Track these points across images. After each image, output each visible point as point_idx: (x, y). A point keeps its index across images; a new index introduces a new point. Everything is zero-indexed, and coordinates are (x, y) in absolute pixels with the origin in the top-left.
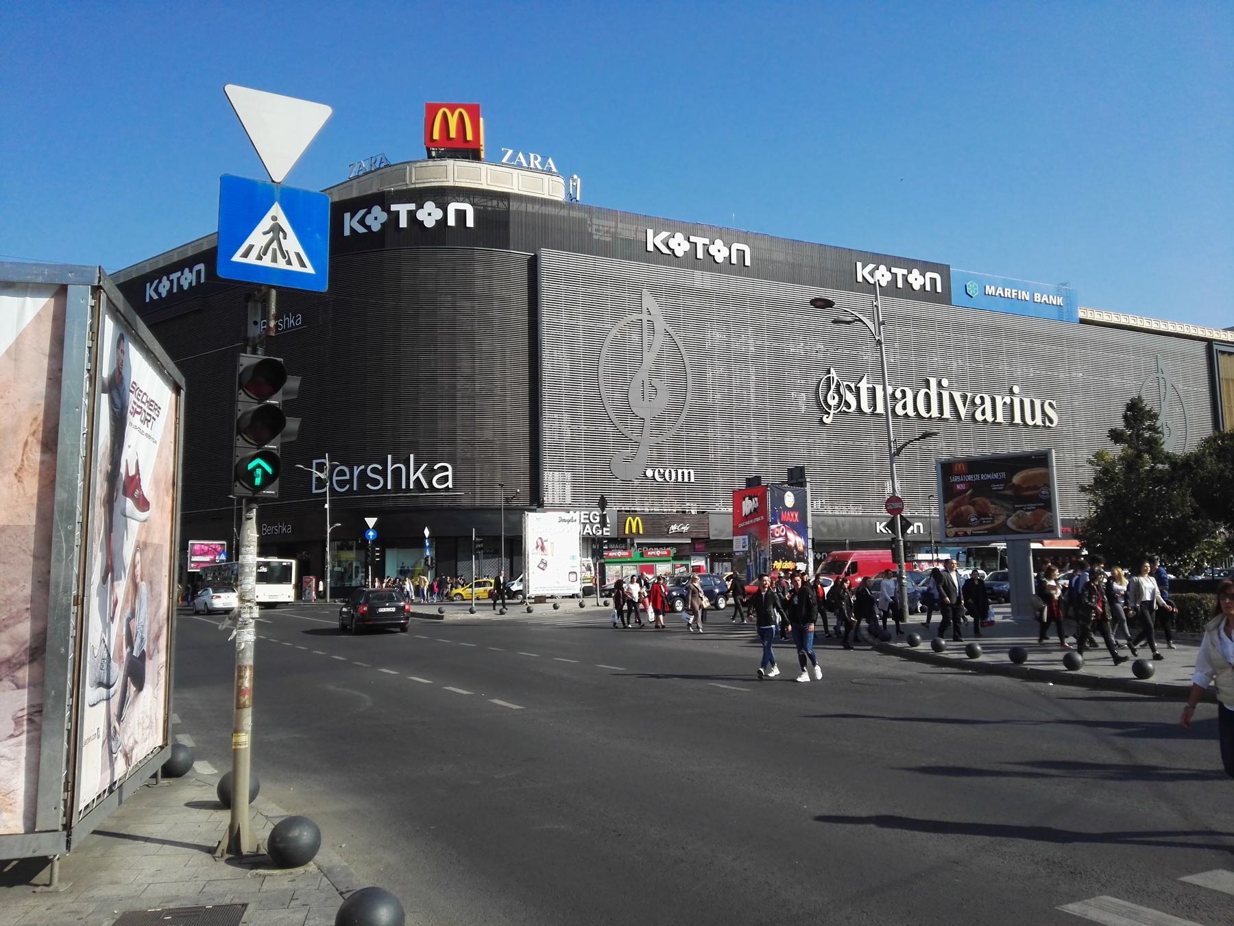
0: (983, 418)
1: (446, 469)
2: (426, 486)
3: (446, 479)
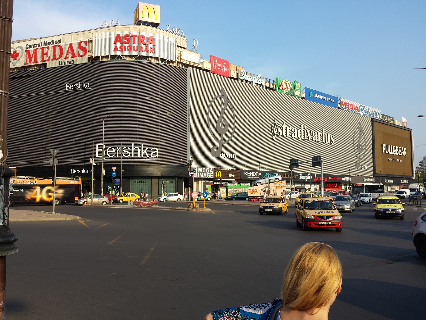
0: (294, 137)
1: (156, 150)
2: (148, 156)
3: (155, 154)
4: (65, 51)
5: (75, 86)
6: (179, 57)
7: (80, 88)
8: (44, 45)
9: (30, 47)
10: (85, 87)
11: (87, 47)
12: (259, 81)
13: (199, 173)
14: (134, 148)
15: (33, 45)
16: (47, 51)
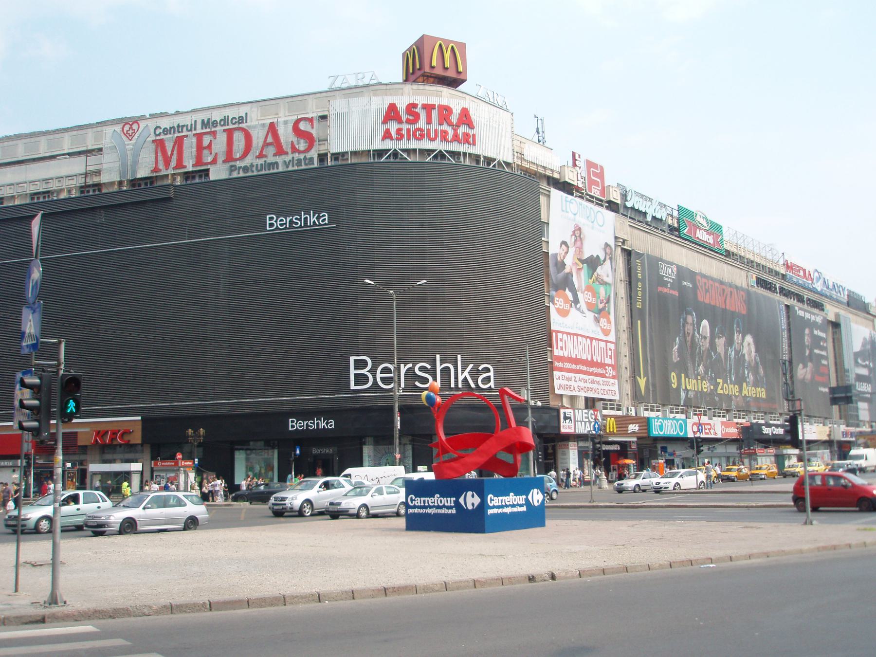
2: (473, 386)
3: (325, 220)
5: (291, 222)
6: (519, 156)
7: (303, 225)
8: (202, 129)
9: (166, 131)
10: (318, 224)
11: (315, 133)
12: (647, 207)
13: (577, 422)
14: (441, 365)
15: (174, 127)
16: (211, 142)
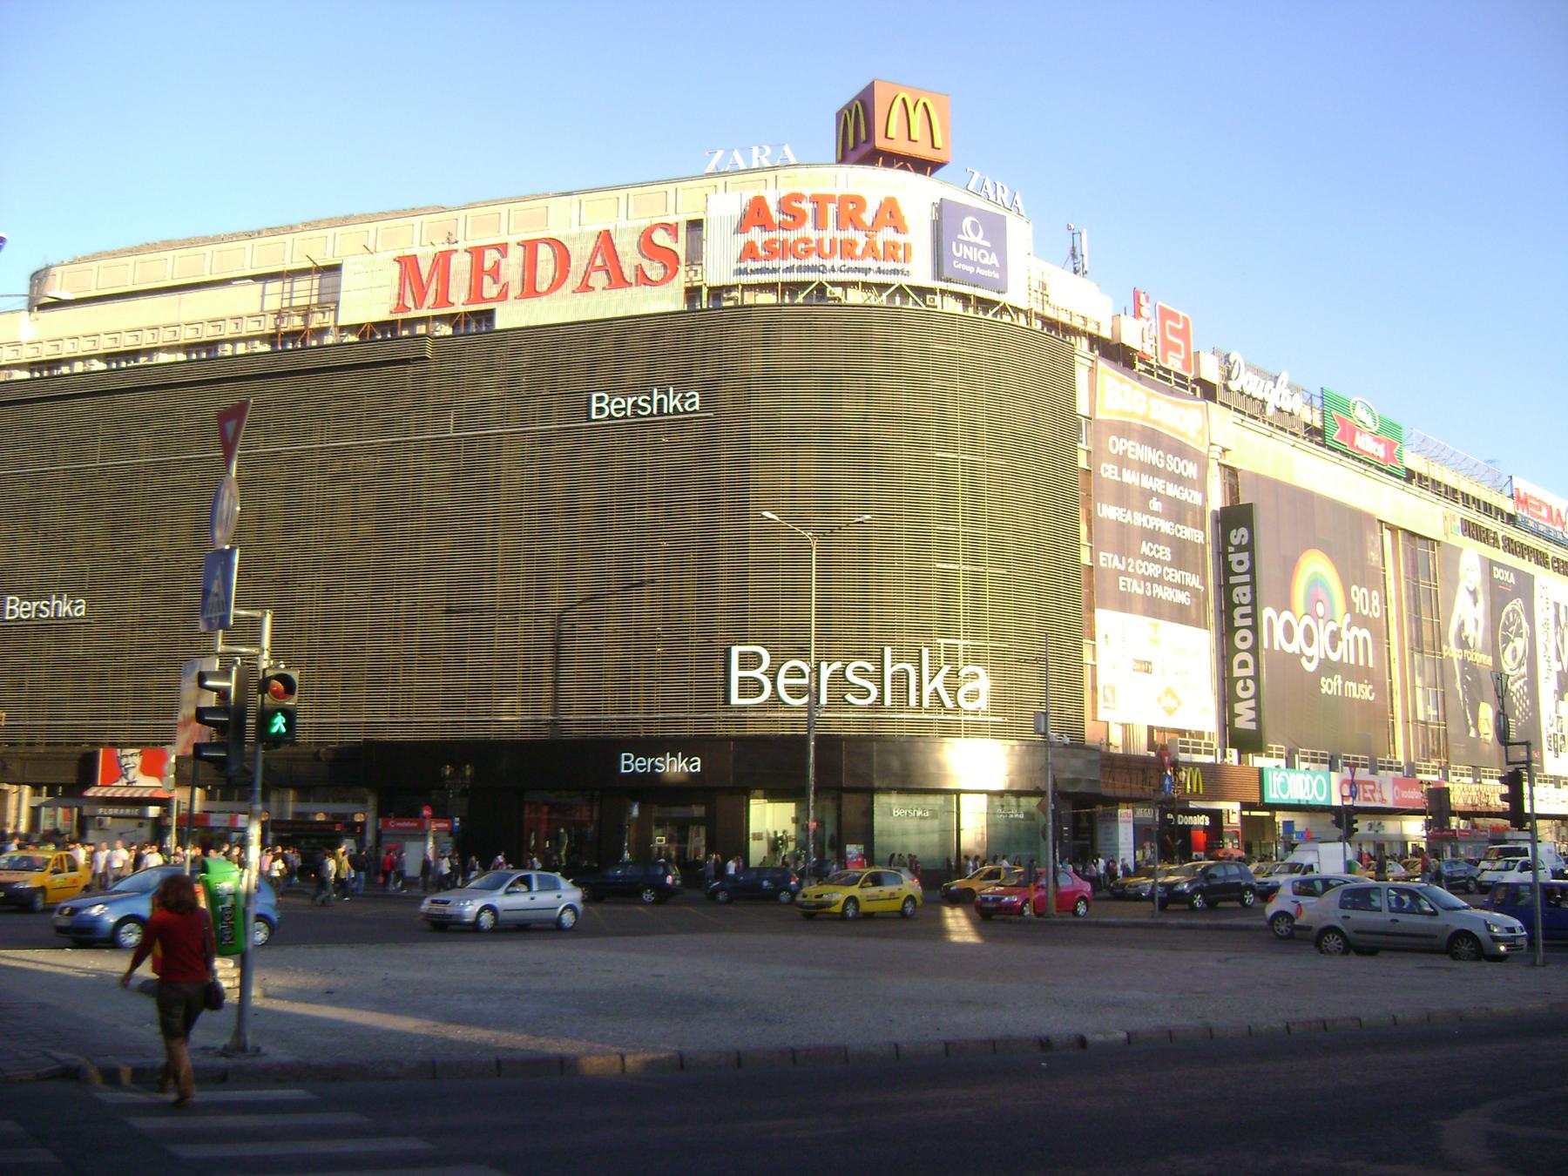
3: (693, 403)
4: (578, 265)
14: (892, 666)
